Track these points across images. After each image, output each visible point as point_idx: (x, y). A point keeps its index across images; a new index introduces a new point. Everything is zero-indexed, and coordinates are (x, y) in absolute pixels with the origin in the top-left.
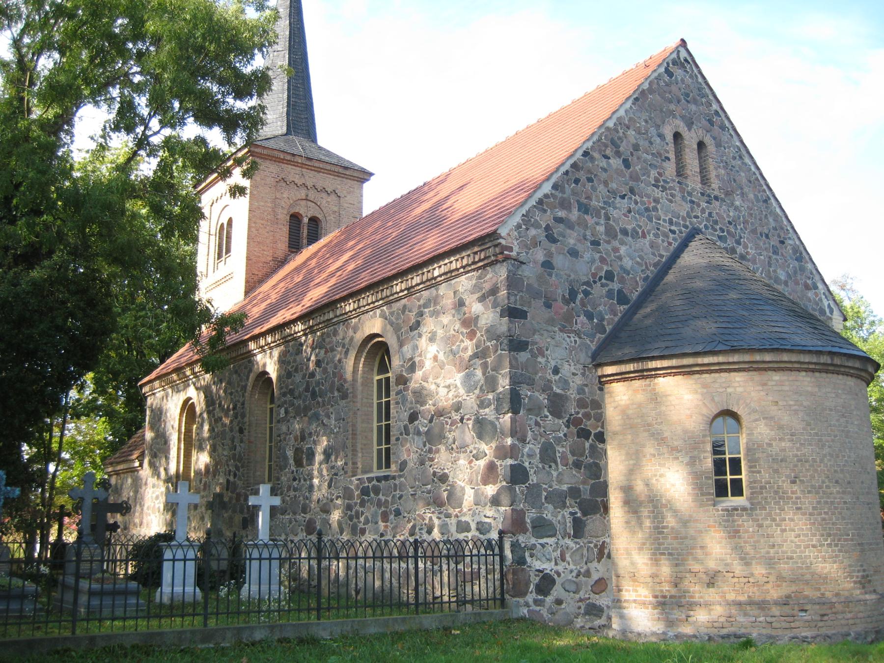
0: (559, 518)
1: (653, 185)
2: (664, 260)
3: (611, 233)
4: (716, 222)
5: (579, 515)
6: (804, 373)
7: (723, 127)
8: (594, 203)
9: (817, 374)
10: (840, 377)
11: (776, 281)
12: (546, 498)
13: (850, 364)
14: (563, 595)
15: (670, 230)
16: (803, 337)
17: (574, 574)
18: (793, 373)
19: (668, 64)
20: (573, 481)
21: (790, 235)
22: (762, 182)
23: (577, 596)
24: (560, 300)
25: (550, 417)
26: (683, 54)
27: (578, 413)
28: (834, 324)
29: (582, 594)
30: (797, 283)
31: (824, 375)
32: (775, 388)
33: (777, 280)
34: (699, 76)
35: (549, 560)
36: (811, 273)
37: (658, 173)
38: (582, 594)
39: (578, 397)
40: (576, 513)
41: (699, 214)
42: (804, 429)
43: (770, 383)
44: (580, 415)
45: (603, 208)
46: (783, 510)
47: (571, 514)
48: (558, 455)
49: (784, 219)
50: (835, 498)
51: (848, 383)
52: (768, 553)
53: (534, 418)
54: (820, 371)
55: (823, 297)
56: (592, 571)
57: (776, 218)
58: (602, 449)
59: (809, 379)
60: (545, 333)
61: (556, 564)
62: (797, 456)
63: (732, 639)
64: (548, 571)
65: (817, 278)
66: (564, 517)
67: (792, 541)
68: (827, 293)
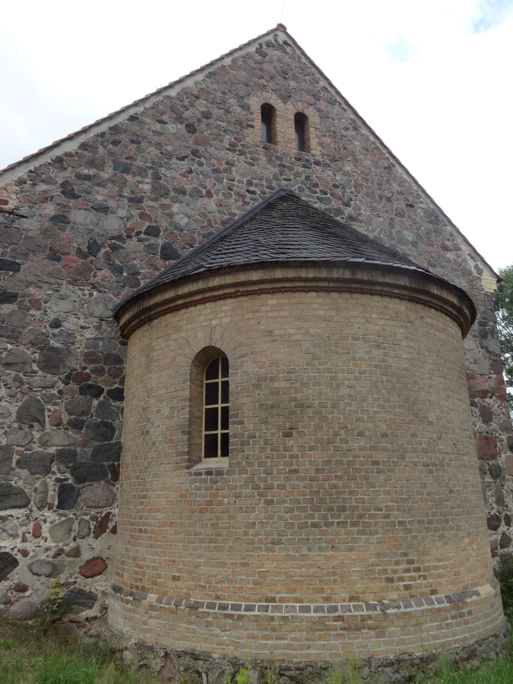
0: (38, 485)
1: (227, 149)
2: (236, 218)
3: (160, 191)
4: (316, 185)
5: (70, 481)
6: (313, 294)
7: (332, 102)
8: (139, 163)
9: (335, 295)
10: (376, 298)
11: (399, 242)
12: (18, 462)
13: (387, 280)
14: (27, 579)
15: (248, 191)
16: (311, 247)
17: (51, 553)
18: (297, 294)
19: (261, 45)
20: (65, 443)
21: (421, 200)
22: (385, 151)
23: (53, 581)
24: (73, 252)
25: (40, 373)
26: (282, 37)
27: (85, 368)
28: (483, 283)
29: (62, 578)
30: (431, 244)
31: (347, 295)
32: (270, 314)
33: (402, 241)
34: (302, 57)
35: (14, 536)
36: (452, 235)
37: (236, 139)
38: (62, 578)
39: (86, 351)
40: (67, 479)
41: (292, 177)
42: (308, 364)
43: (263, 309)
44: (87, 371)
45: (151, 168)
46: (271, 473)
47: (58, 480)
48: (47, 413)
49: (413, 185)
50: (355, 457)
51: (391, 306)
52: (246, 534)
53: (13, 373)
54: (339, 290)
55: (468, 258)
56: (84, 548)
57: (402, 183)
58: (118, 407)
59: (321, 300)
60: (46, 286)
61: (24, 540)
62: (295, 399)
63: (187, 660)
64: (7, 550)
65: (459, 240)
66: (45, 485)
67: (280, 518)
68: (473, 255)
